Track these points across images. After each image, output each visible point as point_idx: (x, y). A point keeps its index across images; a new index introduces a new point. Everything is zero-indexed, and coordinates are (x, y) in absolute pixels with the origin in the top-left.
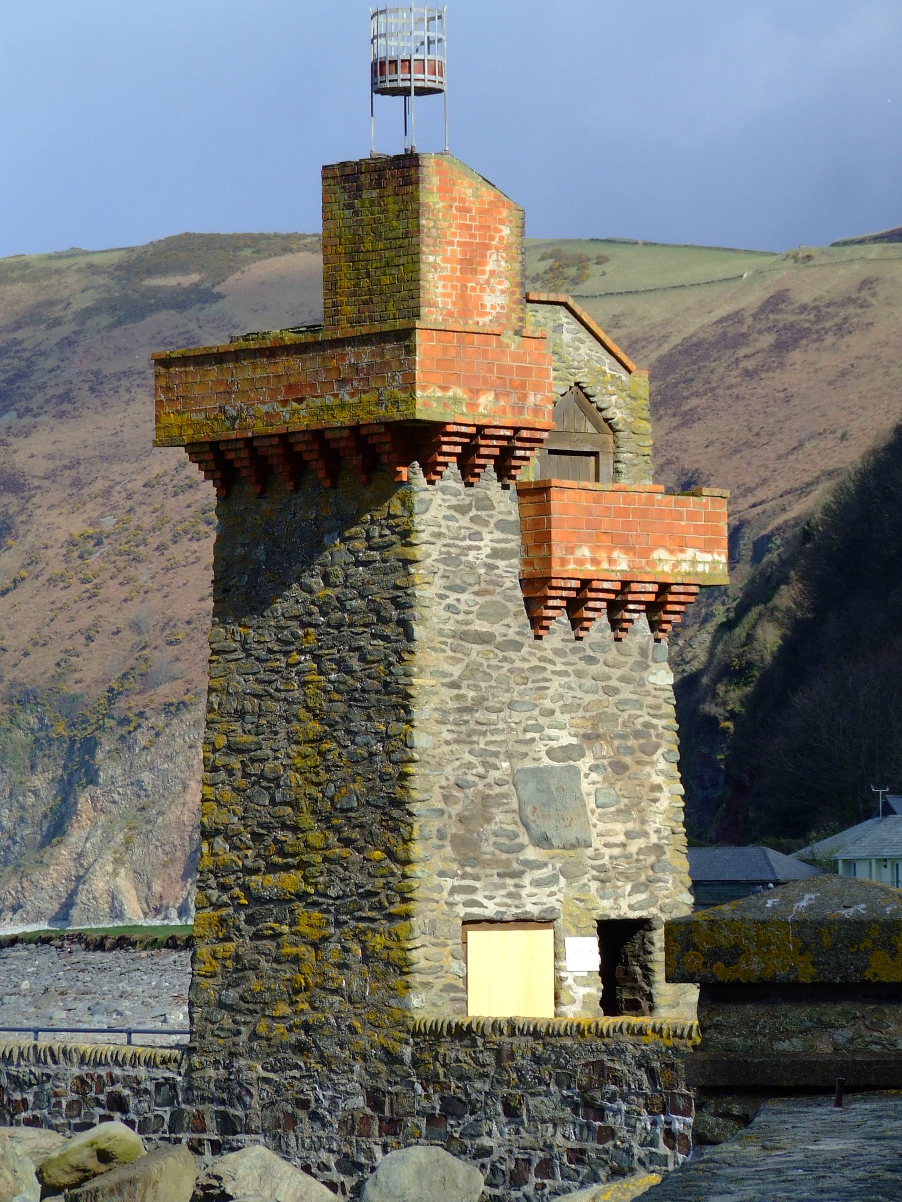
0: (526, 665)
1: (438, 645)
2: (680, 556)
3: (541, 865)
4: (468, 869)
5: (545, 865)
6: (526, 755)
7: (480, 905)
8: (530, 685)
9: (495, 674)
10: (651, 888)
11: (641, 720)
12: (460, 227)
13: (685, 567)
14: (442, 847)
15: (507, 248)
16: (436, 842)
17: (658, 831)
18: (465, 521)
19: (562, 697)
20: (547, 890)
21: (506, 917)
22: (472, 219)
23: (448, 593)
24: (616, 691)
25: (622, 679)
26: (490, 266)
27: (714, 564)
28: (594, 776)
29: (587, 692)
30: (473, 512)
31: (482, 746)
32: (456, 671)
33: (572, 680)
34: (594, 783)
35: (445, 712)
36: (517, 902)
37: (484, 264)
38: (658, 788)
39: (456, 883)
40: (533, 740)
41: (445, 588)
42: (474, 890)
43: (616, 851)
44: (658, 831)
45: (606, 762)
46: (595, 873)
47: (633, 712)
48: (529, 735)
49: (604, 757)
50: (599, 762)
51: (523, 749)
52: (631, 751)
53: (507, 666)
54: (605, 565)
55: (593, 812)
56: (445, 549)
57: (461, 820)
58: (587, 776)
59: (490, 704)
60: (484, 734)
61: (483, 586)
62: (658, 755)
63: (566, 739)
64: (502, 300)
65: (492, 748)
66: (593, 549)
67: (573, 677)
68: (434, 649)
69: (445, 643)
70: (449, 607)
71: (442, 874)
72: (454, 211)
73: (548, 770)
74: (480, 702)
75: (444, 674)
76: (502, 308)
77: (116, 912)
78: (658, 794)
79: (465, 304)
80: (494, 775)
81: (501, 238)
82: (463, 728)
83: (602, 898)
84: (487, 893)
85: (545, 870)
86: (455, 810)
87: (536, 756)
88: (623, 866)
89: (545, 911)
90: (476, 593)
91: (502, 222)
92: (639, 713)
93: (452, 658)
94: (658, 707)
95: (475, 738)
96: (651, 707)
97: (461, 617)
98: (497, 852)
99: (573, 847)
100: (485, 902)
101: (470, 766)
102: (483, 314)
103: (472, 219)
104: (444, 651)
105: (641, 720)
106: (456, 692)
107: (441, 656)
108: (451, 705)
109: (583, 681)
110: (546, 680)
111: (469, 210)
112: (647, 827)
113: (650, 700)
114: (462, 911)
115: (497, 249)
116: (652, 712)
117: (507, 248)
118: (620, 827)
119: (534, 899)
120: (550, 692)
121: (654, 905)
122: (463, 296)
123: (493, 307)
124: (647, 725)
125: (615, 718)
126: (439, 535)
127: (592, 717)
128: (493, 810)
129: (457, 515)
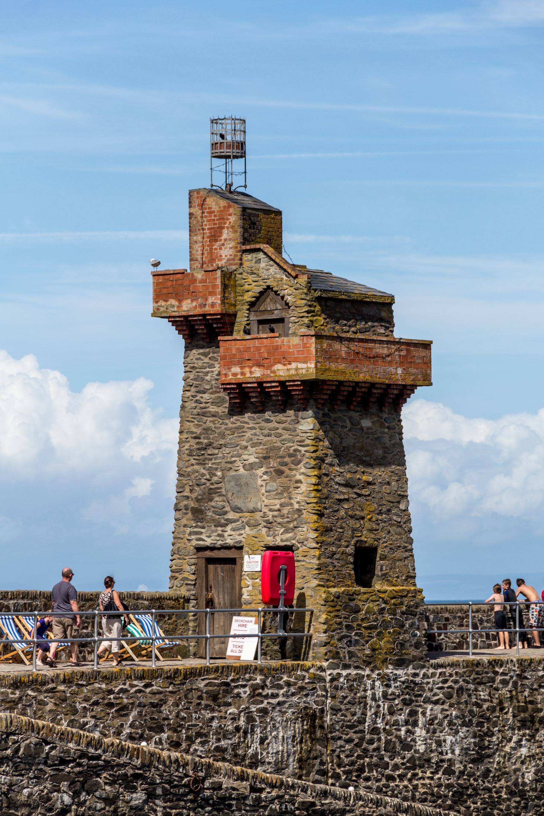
0: (234, 426)
1: (190, 419)
2: (289, 367)
3: (235, 521)
4: (199, 524)
5: (238, 520)
6: (231, 468)
7: (204, 540)
8: (235, 435)
9: (217, 431)
10: (295, 531)
11: (293, 448)
12: (208, 221)
13: (293, 372)
14: (187, 513)
15: (233, 227)
16: (184, 511)
17: (298, 503)
18: (206, 360)
19: (251, 440)
20: (238, 532)
21: (217, 546)
22: (215, 216)
23: (197, 394)
24: (281, 435)
25: (284, 429)
26: (224, 236)
27: (308, 369)
28: (265, 477)
29: (265, 436)
30: (211, 355)
31: (210, 465)
32: (198, 431)
33: (258, 431)
34: (264, 480)
35: (191, 451)
36: (222, 539)
37: (220, 236)
38: (300, 481)
39: (192, 530)
40: (235, 461)
41: (196, 392)
42: (201, 533)
43: (276, 513)
44: (298, 503)
45: (272, 469)
46: (265, 524)
47: (288, 445)
48: (233, 459)
49: (271, 467)
50: (268, 470)
51: (229, 466)
52: (286, 464)
53: (223, 427)
54: (248, 375)
55: (263, 495)
56: (197, 374)
57: (197, 500)
58: (261, 477)
59: (215, 445)
60: (211, 459)
61: (214, 389)
62: (301, 465)
63: (252, 459)
64: (231, 252)
65: (214, 466)
66: (242, 368)
67: (258, 430)
68: (188, 421)
69: (195, 418)
70: (197, 401)
71: (185, 526)
72: (206, 214)
73: (241, 475)
74: (210, 444)
75: (192, 433)
76: (231, 255)
77: (222, 569)
78: (299, 485)
79: (211, 257)
80: (215, 479)
81: (230, 223)
82: (201, 457)
83: (268, 536)
84: (208, 535)
85: (238, 523)
86: (194, 496)
87: (237, 468)
88: (279, 520)
89: (237, 542)
90: (212, 393)
91: (230, 215)
92: (292, 445)
93: (197, 425)
94: (303, 441)
95: (207, 462)
96: (298, 441)
97: (202, 405)
98: (214, 515)
99: (252, 512)
100: (206, 539)
101: (203, 475)
102: (220, 260)
103: (215, 216)
104: (193, 422)
105: (293, 448)
106: (198, 440)
107: (192, 424)
108: (196, 447)
109: (263, 431)
110: (244, 432)
111: (214, 212)
112: (292, 501)
113: (298, 438)
114: (194, 543)
115: (228, 228)
116: (299, 444)
117: (233, 227)
118: (277, 502)
119: (231, 537)
120: (246, 438)
121: (294, 539)
122: (211, 253)
123: (226, 256)
124: (295, 450)
125: (279, 448)
126: (193, 368)
127: (267, 449)
128: (214, 495)
129: (202, 357)
